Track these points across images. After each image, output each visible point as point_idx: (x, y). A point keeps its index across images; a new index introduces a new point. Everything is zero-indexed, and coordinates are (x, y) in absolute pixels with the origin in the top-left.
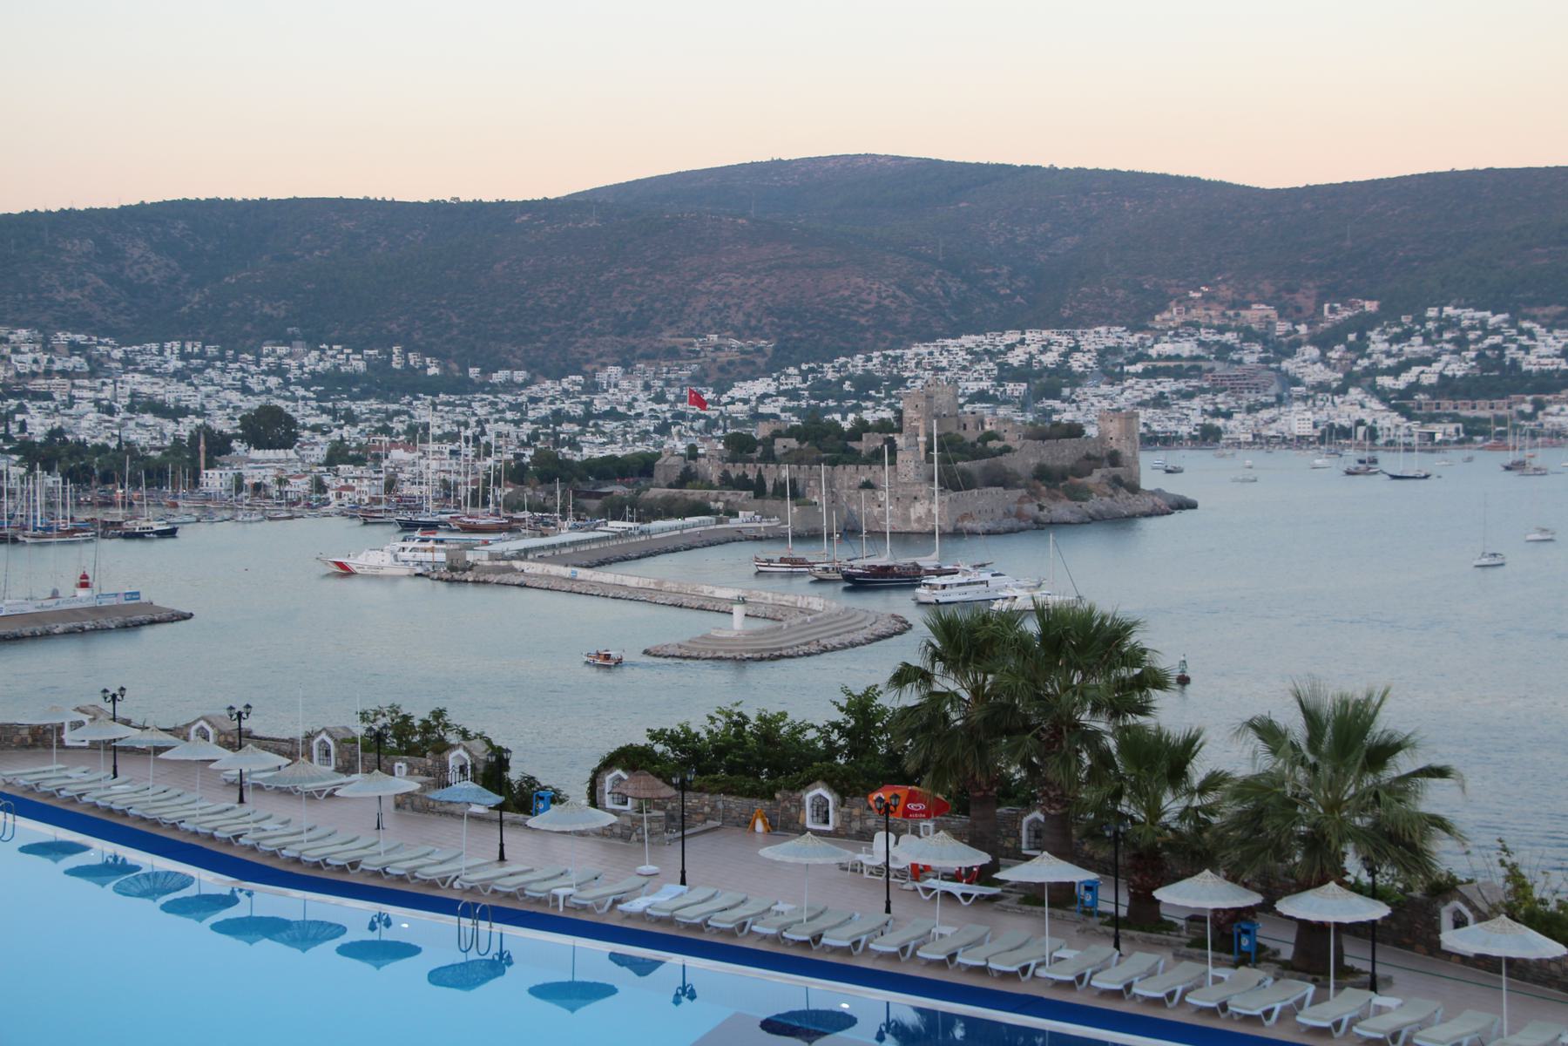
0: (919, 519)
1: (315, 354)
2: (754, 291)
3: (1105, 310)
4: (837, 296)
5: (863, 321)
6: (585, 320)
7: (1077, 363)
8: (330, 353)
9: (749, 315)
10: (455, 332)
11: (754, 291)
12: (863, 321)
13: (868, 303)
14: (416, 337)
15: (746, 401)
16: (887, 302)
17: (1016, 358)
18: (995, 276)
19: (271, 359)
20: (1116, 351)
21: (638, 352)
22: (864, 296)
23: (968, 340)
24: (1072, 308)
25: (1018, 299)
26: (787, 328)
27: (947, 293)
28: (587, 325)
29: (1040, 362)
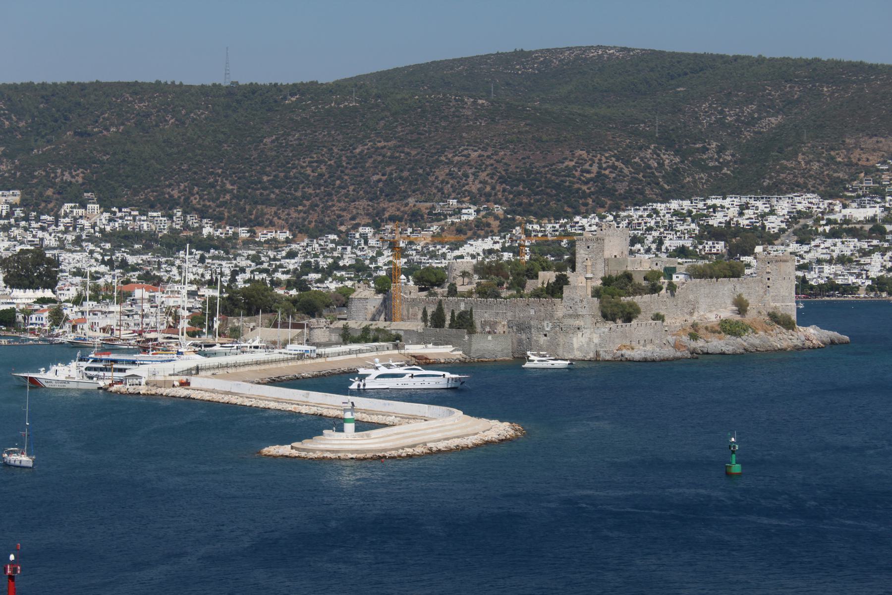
0: (579, 349)
1: (107, 215)
2: (488, 162)
3: (801, 181)
4: (563, 166)
5: (585, 188)
6: (340, 187)
7: (774, 224)
8: (119, 214)
9: (484, 183)
10: (228, 197)
11: (488, 162)
12: (585, 188)
13: (588, 172)
14: (194, 202)
15: (473, 257)
16: (607, 172)
17: (717, 220)
18: (705, 150)
19: (67, 220)
20: (807, 215)
21: (387, 215)
22: (587, 166)
23: (674, 205)
24: (771, 178)
25: (725, 170)
26: (519, 193)
27: (661, 165)
28: (343, 191)
29: (738, 223)
